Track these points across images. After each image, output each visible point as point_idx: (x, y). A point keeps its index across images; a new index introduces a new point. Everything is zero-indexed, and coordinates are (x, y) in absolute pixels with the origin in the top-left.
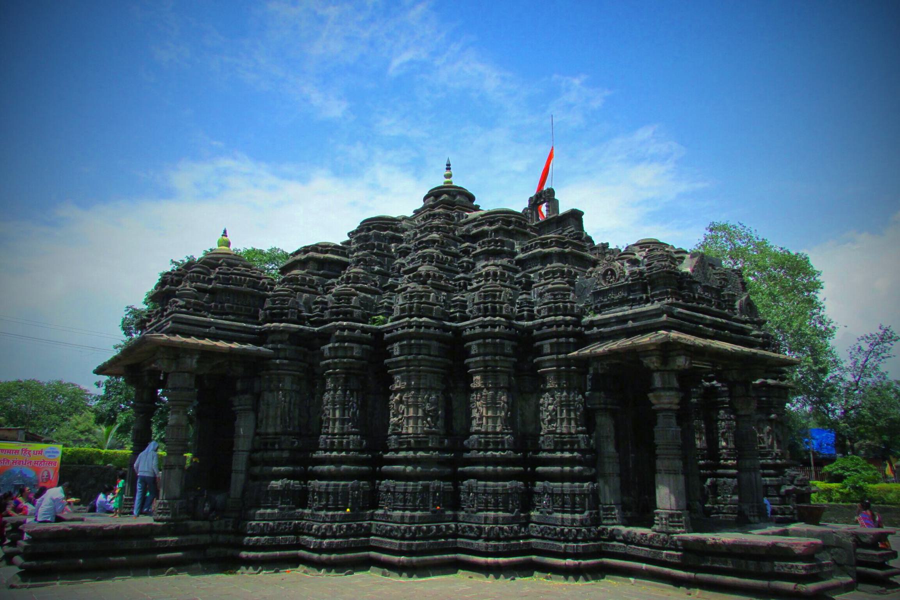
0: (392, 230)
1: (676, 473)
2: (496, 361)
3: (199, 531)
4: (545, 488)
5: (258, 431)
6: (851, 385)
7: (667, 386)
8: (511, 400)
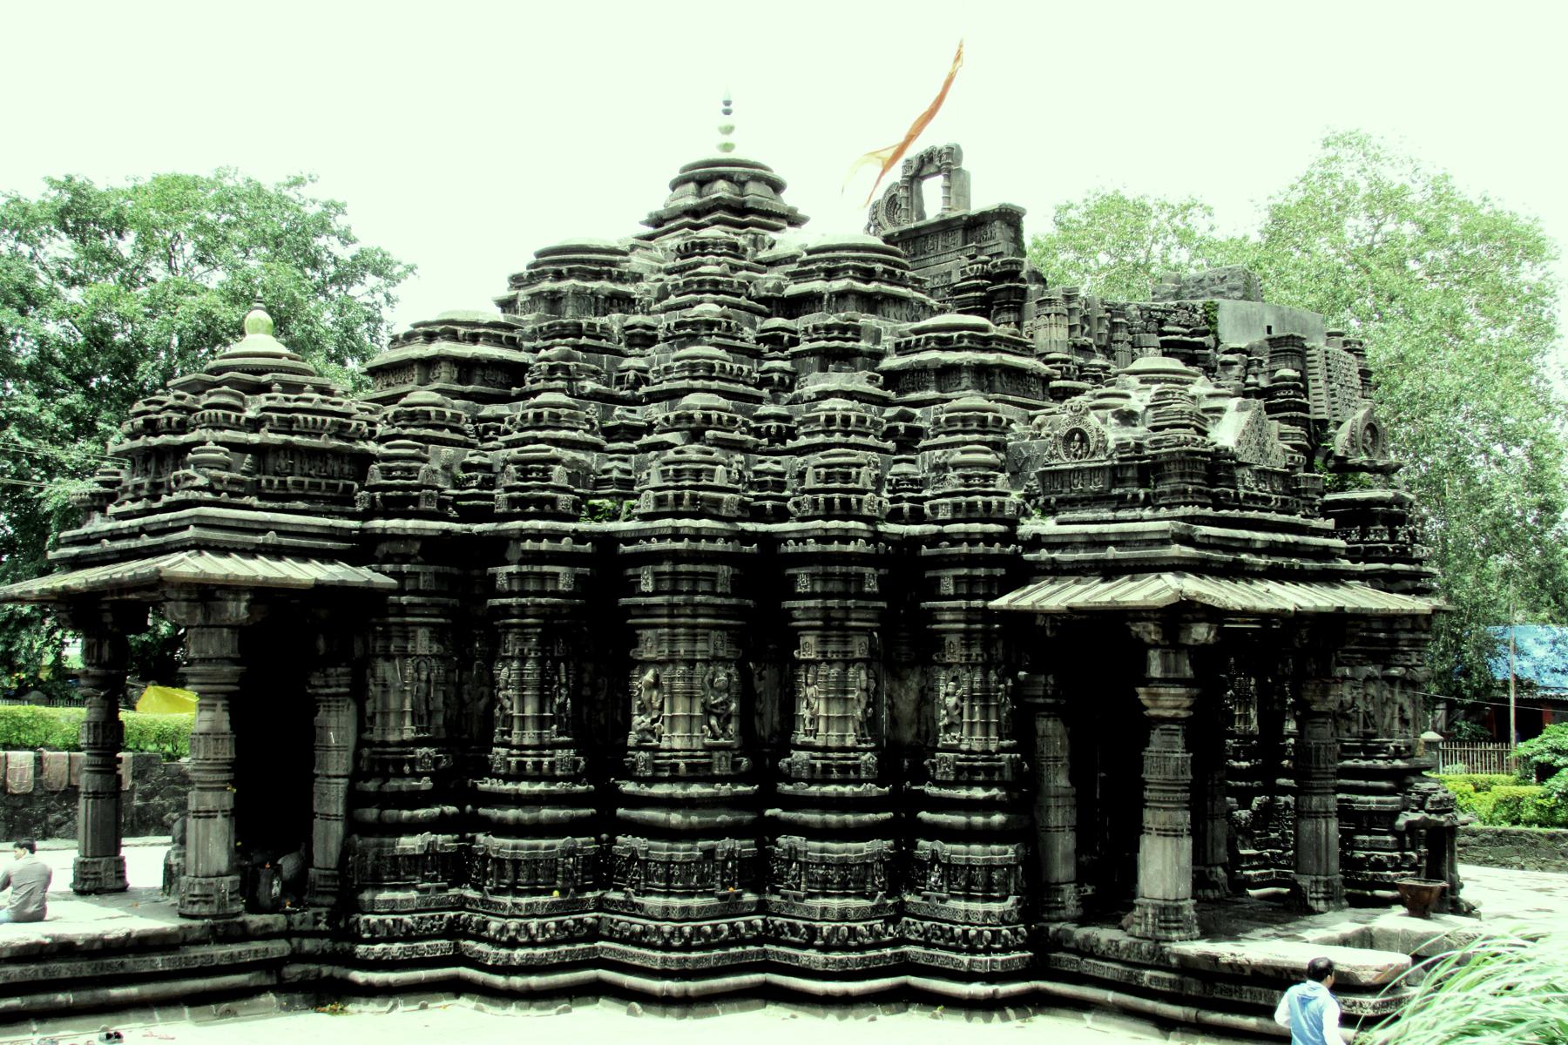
0: (611, 278)
1: (1177, 834)
2: (847, 609)
3: (266, 934)
4: (934, 853)
5: (367, 736)
7: (1171, 676)
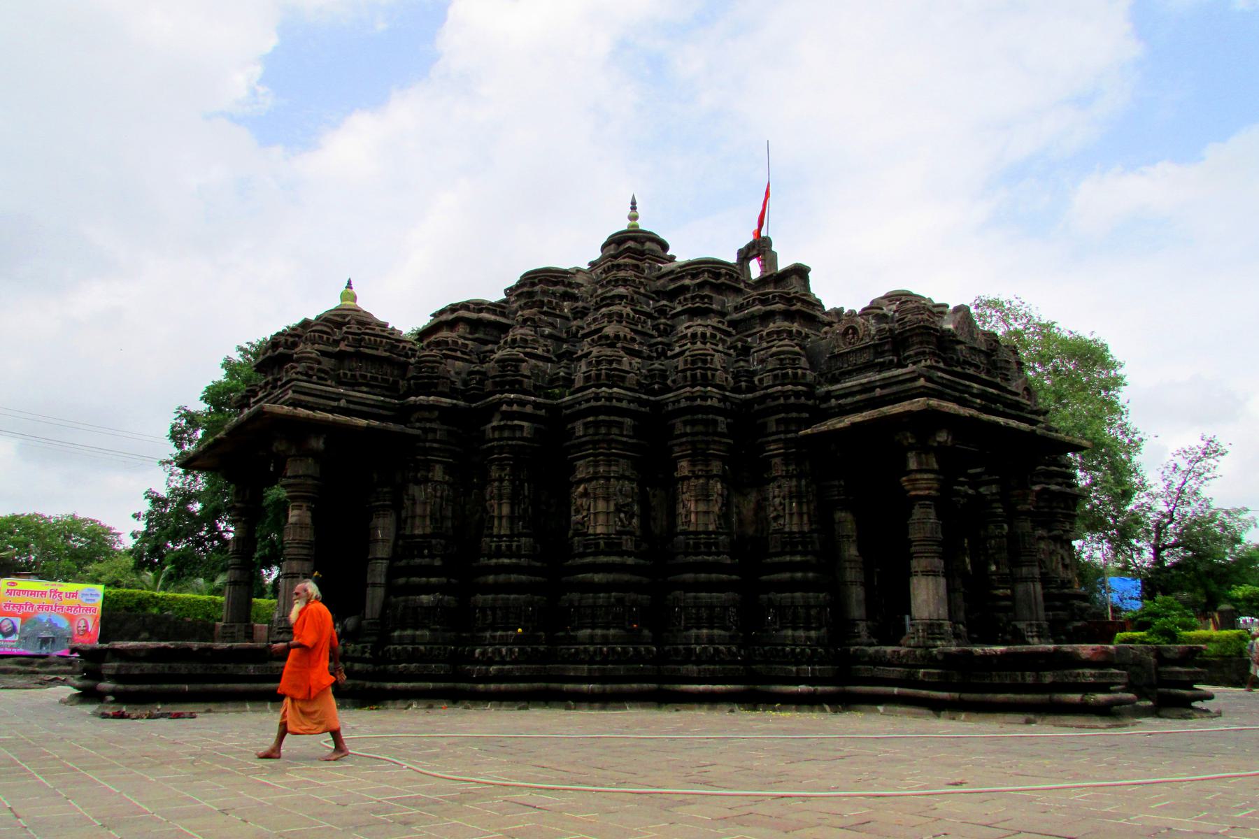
1: (934, 573)
6: (1164, 516)
8: (726, 492)
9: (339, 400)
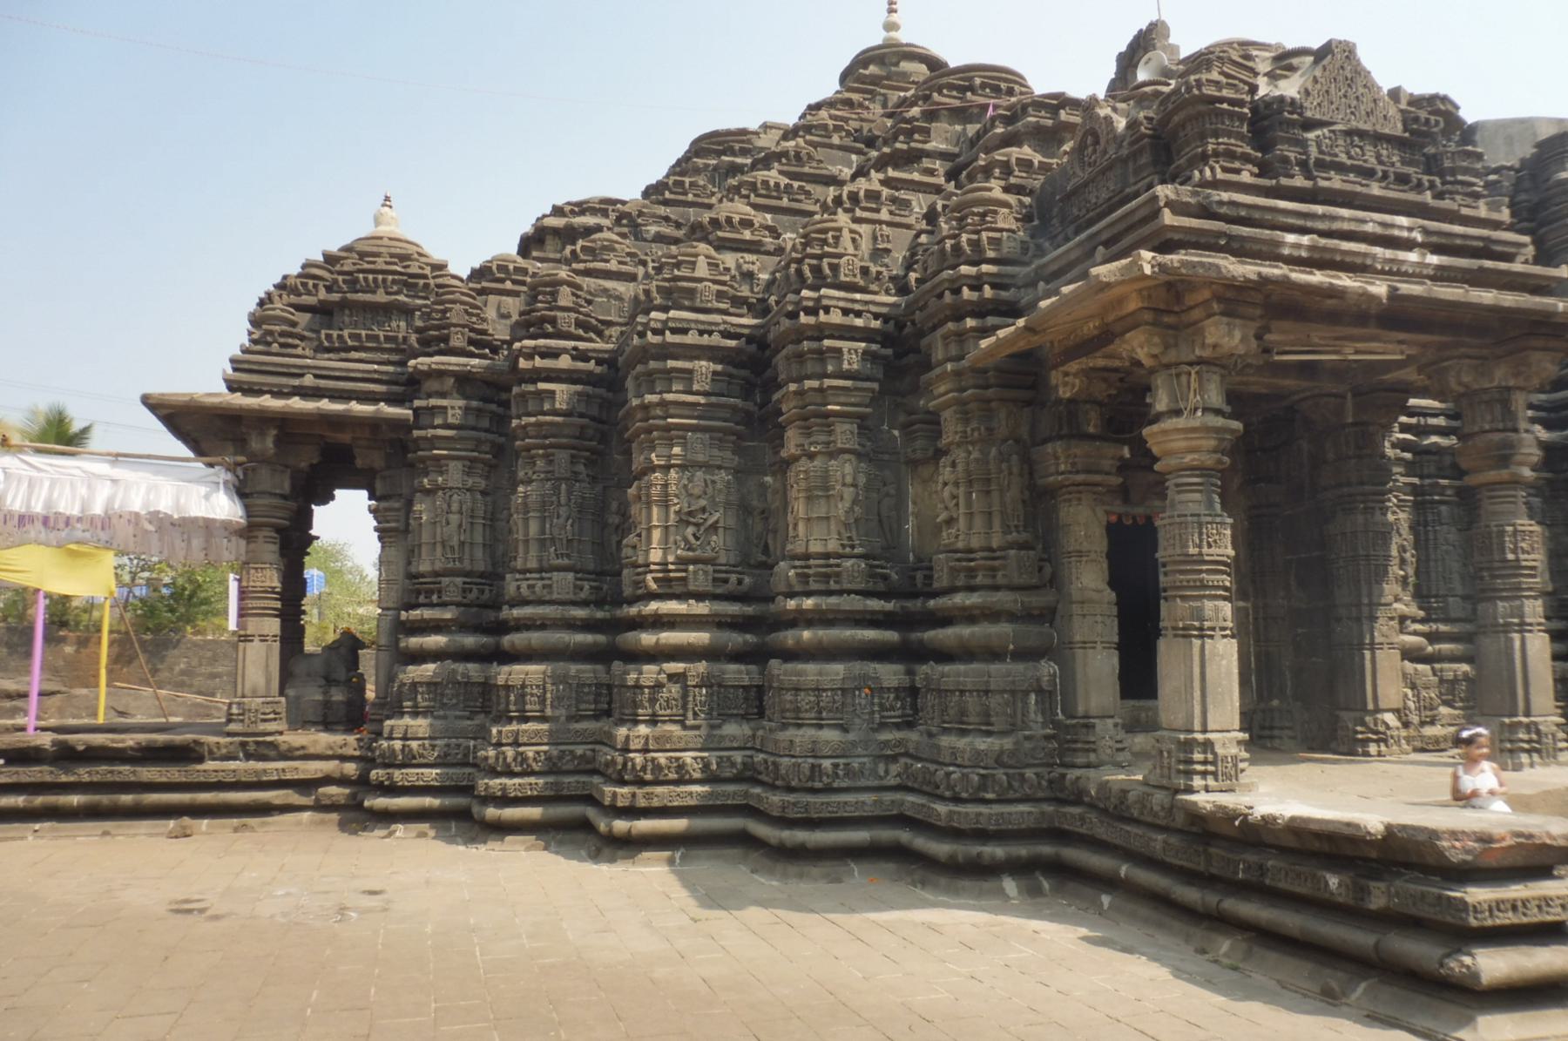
5: (413, 570)
9: (302, 375)
